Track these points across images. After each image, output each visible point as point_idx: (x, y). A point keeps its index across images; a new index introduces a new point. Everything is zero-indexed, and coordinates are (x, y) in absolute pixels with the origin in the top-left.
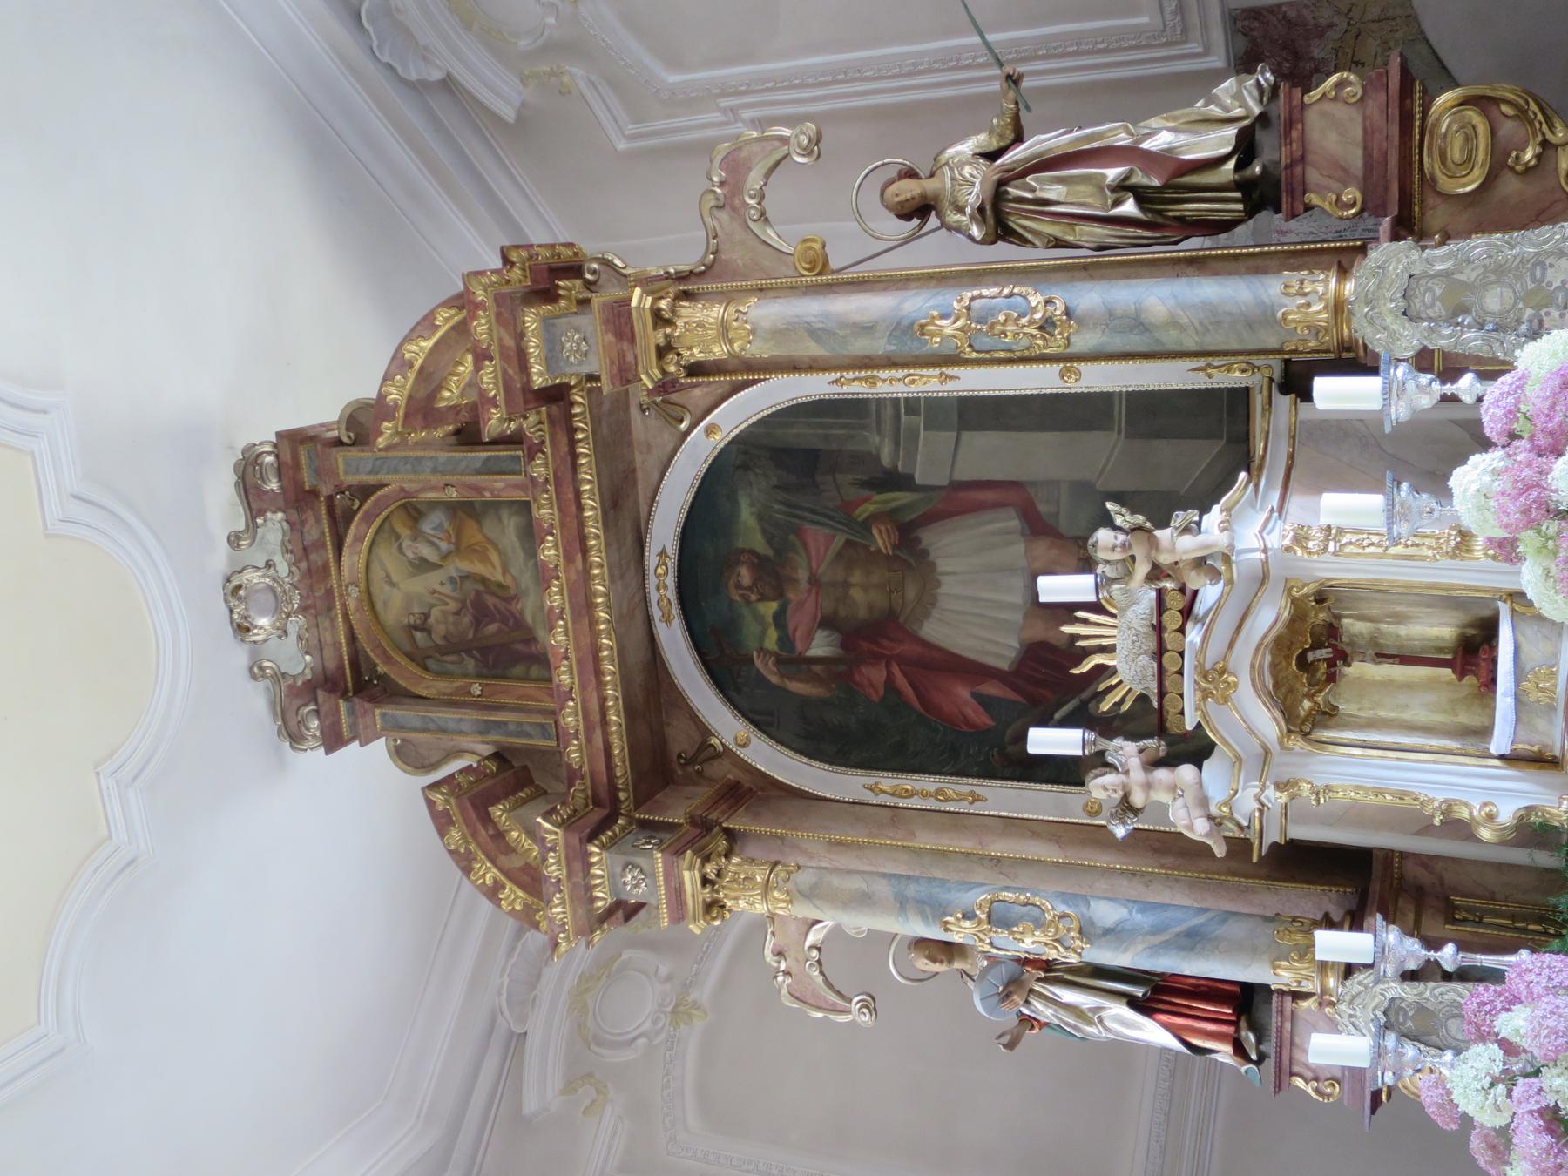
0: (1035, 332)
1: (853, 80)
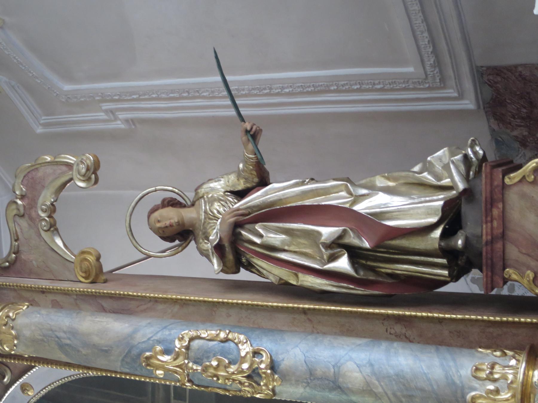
0: (244, 380)
1: (194, 98)
